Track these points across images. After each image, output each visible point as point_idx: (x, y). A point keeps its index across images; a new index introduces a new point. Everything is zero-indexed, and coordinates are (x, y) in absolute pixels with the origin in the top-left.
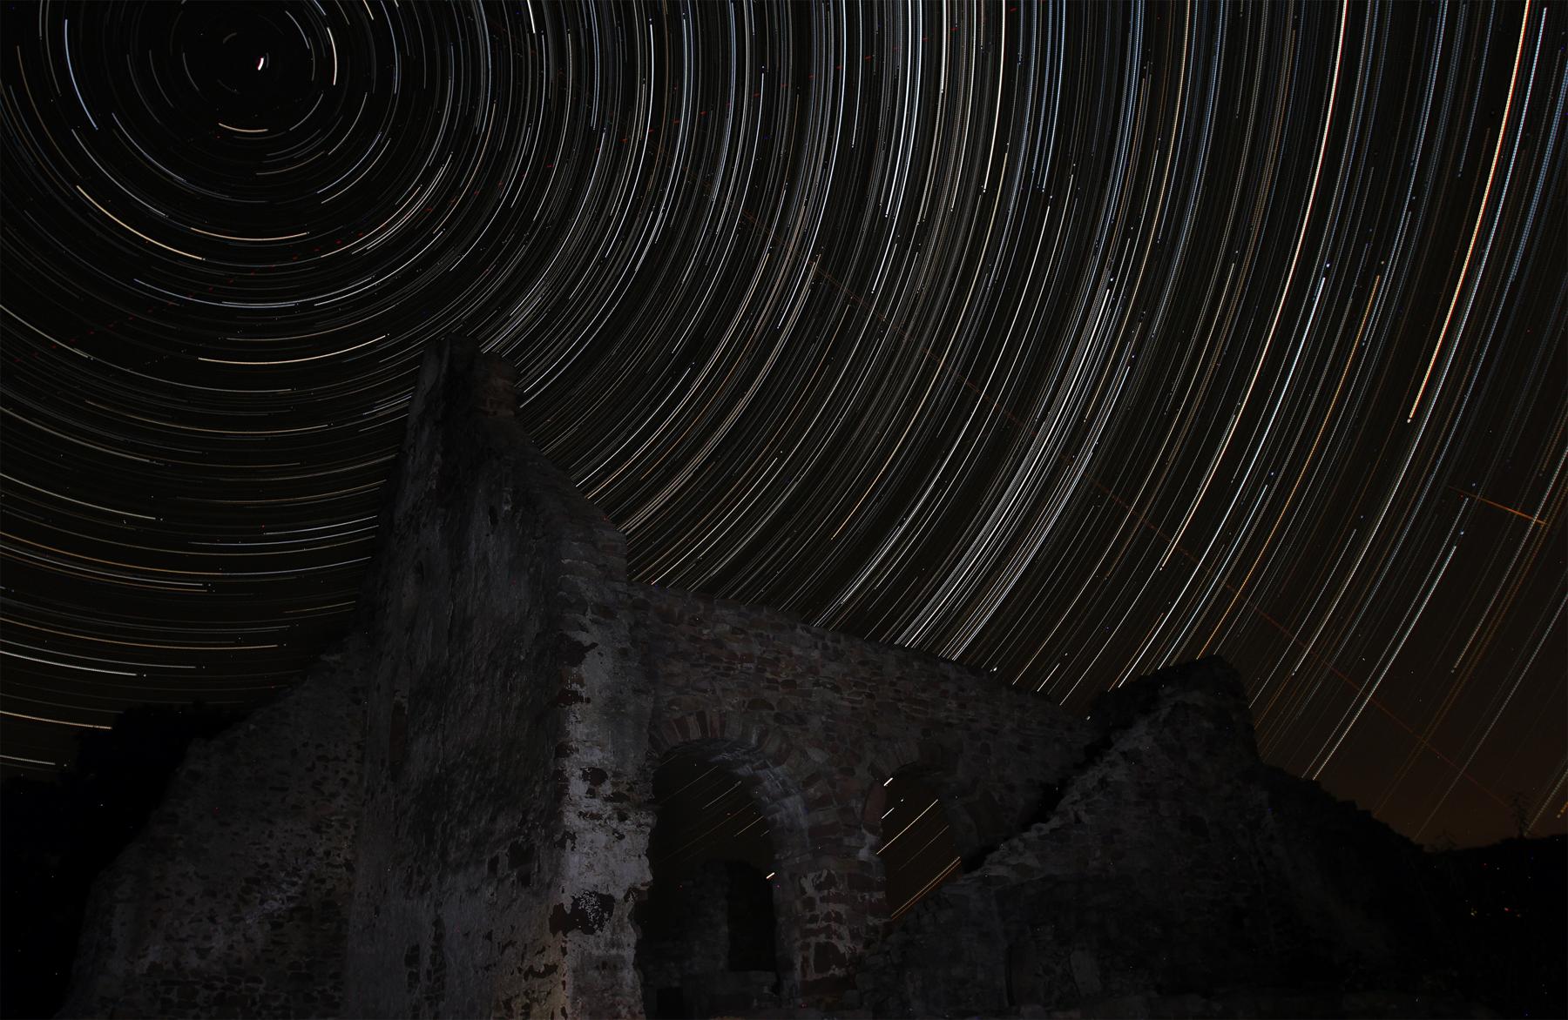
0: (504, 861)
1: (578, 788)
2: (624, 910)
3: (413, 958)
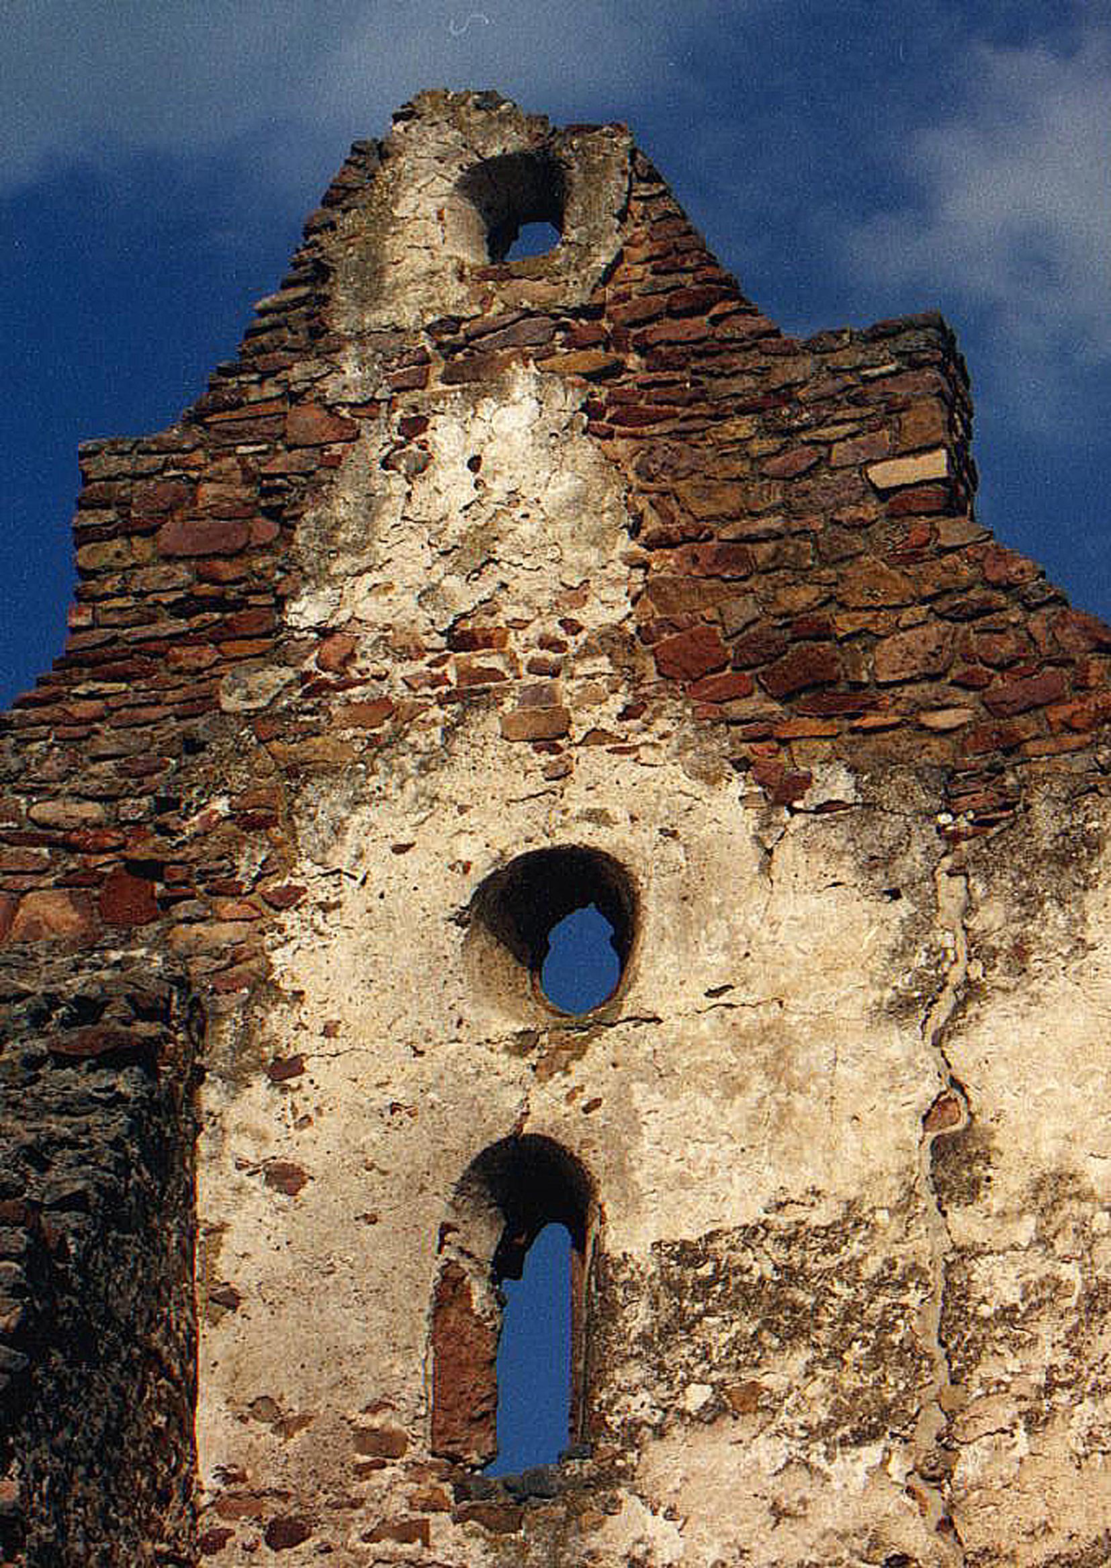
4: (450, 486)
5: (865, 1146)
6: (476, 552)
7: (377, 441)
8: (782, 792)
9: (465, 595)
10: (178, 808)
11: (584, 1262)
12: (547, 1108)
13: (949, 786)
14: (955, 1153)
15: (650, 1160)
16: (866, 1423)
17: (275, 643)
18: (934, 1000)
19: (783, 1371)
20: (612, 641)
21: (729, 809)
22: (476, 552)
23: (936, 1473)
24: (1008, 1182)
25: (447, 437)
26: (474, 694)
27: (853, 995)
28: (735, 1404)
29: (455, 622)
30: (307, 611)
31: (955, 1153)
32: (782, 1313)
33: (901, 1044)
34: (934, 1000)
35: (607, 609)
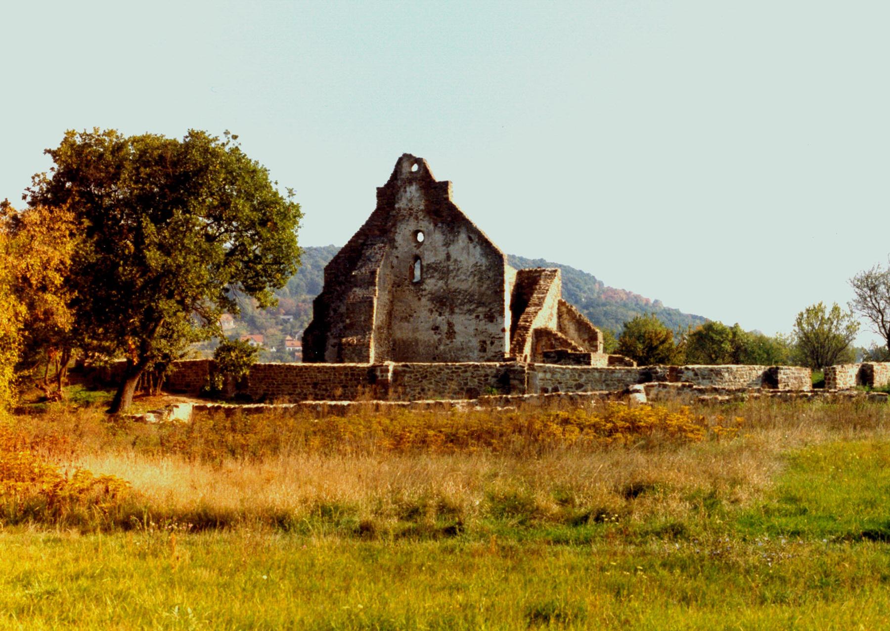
0: (481, 316)
4: (408, 194)
5: (442, 256)
6: (410, 201)
7: (402, 190)
8: (436, 225)
9: (410, 205)
10: (229, 208)
11: (489, 360)
12: (418, 252)
13: (448, 225)
14: (448, 257)
15: (426, 257)
16: (441, 278)
17: (394, 209)
18: (447, 244)
19: (435, 274)
20: (422, 210)
21: (431, 227)
22: (410, 201)
23: (446, 283)
24: (452, 260)
25: (408, 189)
26: (411, 215)
27: (440, 243)
28: (432, 277)
29: (92, 485)
30: (397, 206)
31: (448, 257)
32: (435, 270)
33: (444, 248)
34: (447, 244)
35: (422, 207)
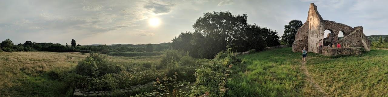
1: (320, 34)
2: (322, 40)
3: (312, 40)
